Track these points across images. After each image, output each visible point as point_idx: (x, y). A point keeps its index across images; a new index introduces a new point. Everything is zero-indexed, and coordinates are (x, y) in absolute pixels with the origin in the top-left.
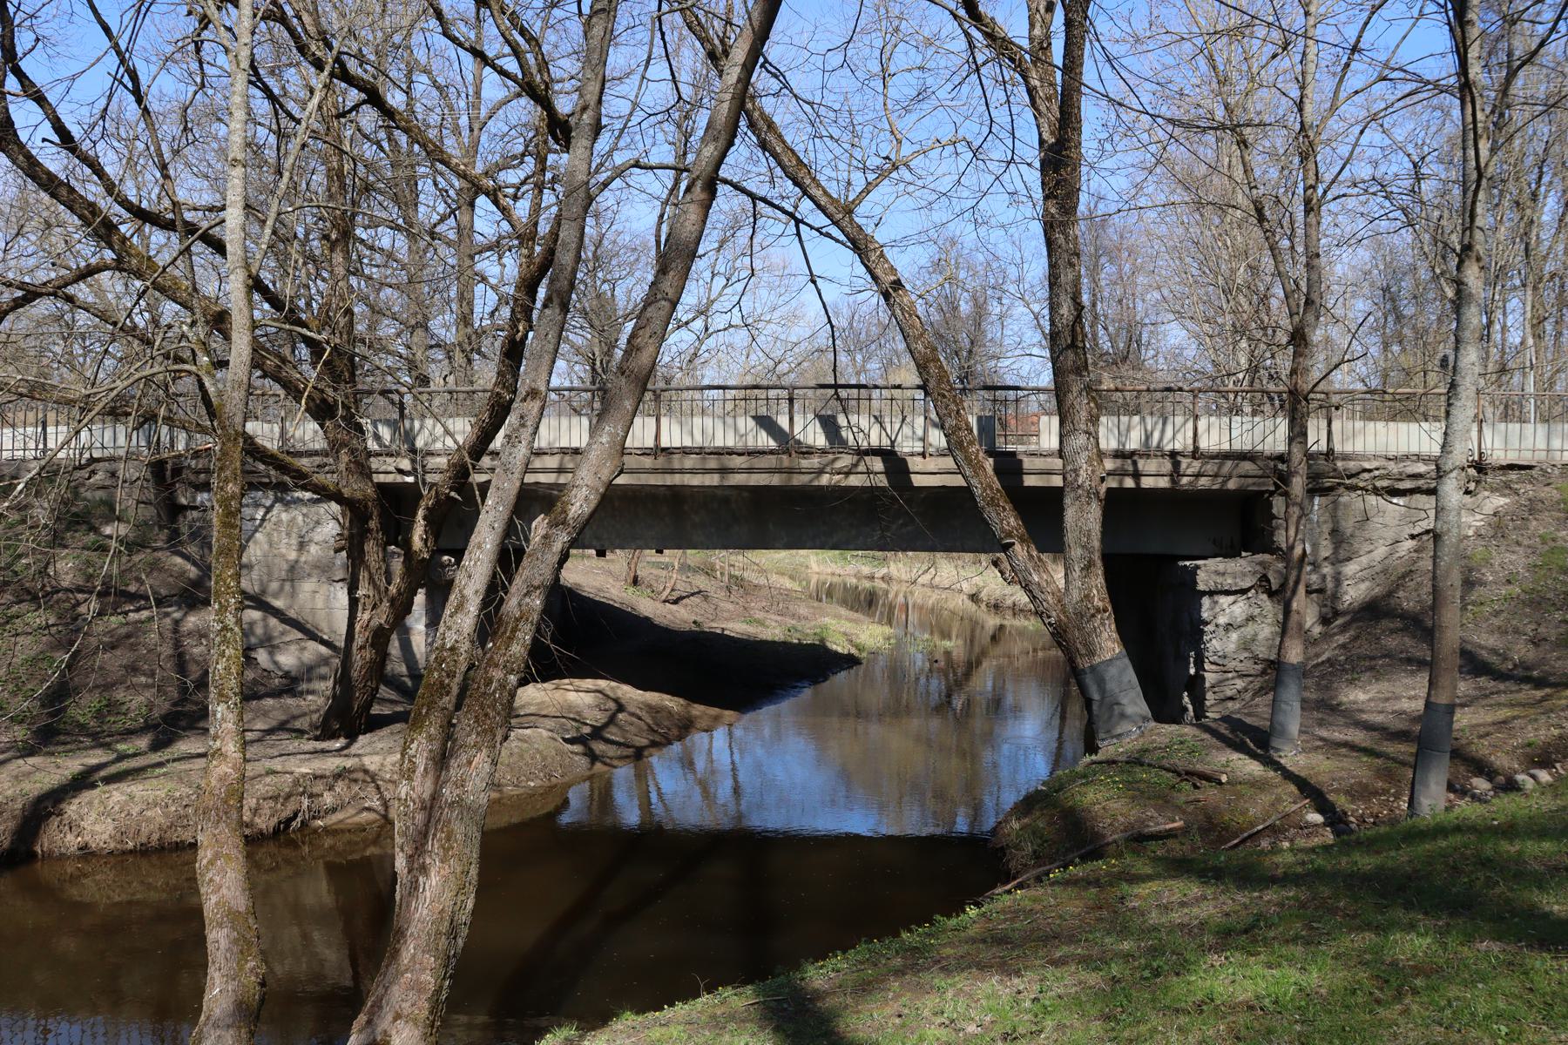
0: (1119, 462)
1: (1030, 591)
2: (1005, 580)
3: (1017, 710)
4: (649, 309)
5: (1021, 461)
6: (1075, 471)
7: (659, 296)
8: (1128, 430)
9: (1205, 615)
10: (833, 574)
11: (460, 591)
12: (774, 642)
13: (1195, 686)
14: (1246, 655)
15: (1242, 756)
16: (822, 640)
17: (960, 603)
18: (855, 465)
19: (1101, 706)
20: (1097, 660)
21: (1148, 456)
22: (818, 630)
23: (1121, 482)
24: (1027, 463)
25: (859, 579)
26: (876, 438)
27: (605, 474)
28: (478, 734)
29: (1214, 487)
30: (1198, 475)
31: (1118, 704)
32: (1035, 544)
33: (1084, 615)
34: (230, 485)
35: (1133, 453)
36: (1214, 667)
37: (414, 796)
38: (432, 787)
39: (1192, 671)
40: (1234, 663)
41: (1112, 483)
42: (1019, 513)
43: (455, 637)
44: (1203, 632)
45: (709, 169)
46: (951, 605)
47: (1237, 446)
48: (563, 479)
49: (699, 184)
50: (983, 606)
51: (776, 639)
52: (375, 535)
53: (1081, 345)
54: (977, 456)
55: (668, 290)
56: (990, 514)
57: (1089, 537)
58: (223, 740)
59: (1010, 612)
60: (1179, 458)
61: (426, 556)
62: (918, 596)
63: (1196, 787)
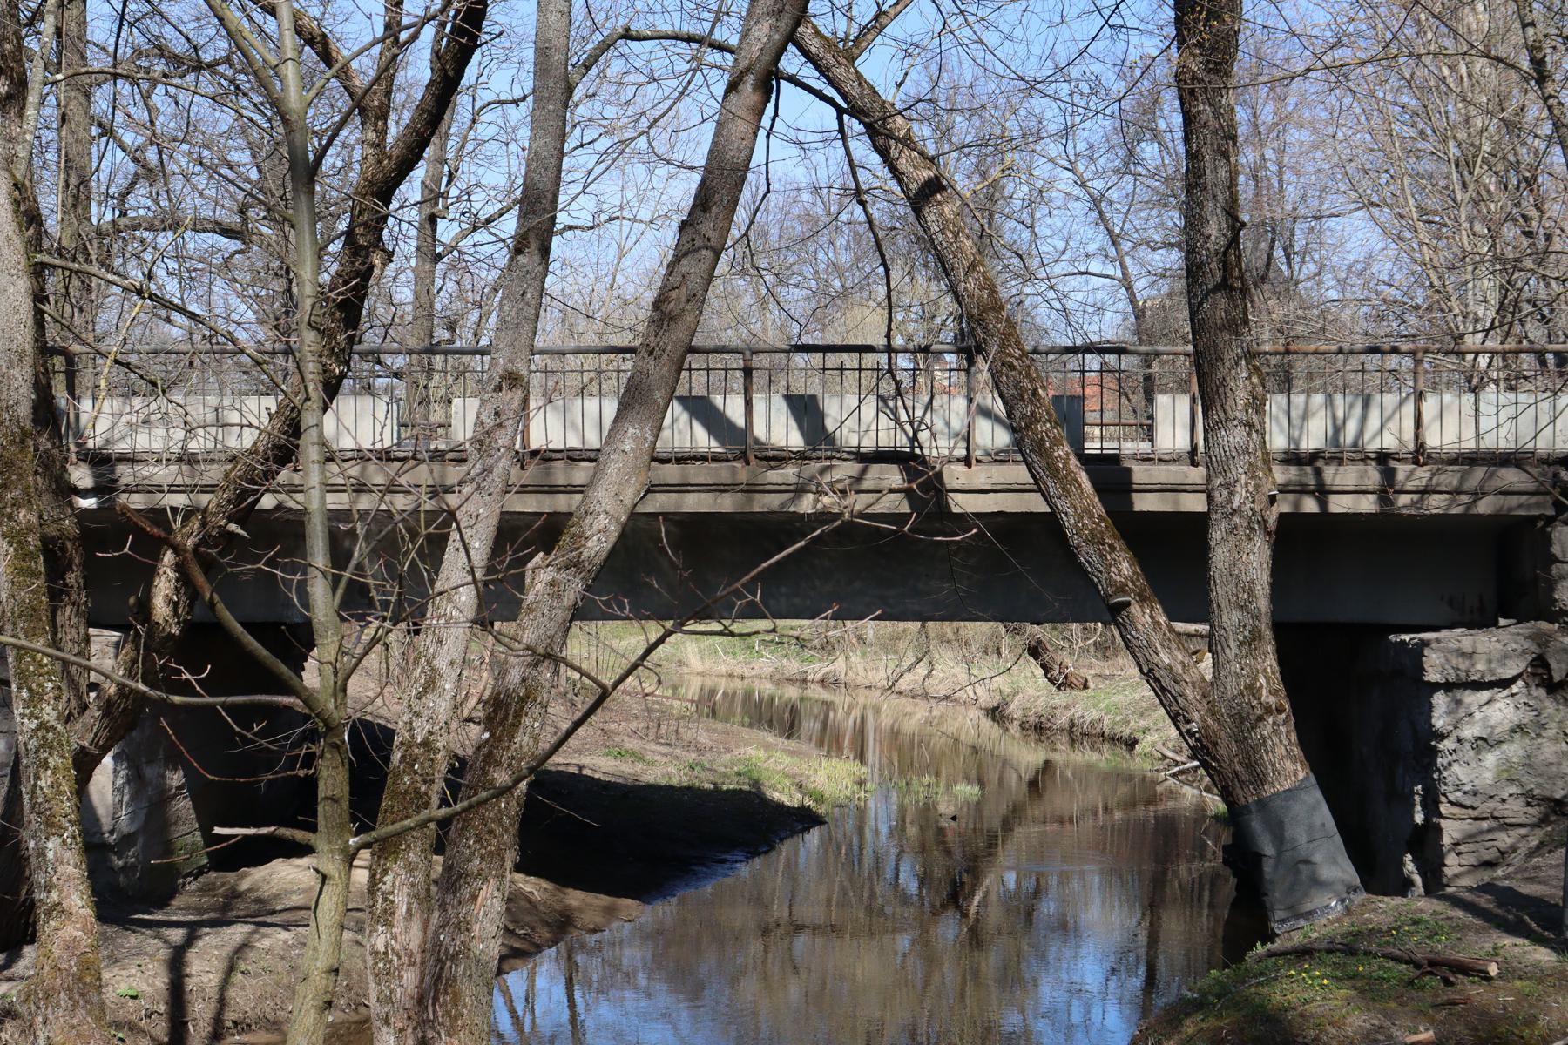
0: (1293, 471)
1: (1157, 680)
2: (1051, 681)
3: (1065, 928)
4: (684, 261)
5: (1129, 471)
6: (1227, 486)
7: (698, 243)
8: (1305, 416)
9: (1440, 721)
10: (730, 675)
11: (429, 663)
12: (671, 788)
13: (1426, 843)
14: (1513, 790)
15: (1519, 941)
16: (756, 783)
17: (970, 724)
18: (859, 479)
19: (1276, 867)
20: (1269, 790)
21: (1340, 462)
22: (742, 768)
23: (1297, 504)
24: (1140, 474)
25: (778, 683)
26: (885, 435)
27: (629, 496)
28: (482, 858)
29: (1455, 511)
30: (1425, 492)
31: (1307, 862)
32: (1161, 603)
33: (1244, 721)
34: (23, 512)
35: (1315, 456)
36: (1456, 810)
37: (397, 947)
38: (420, 934)
39: (1419, 818)
40: (1491, 804)
41: (1284, 507)
42: (1136, 555)
43: (428, 727)
44: (1435, 752)
45: (766, 59)
46: (951, 727)
47: (1488, 443)
48: (561, 503)
49: (750, 79)
50: (1014, 729)
51: (675, 782)
52: (74, 597)
53: (1238, 284)
54: (1066, 464)
55: (710, 233)
56: (1088, 555)
57: (1251, 592)
58: (61, 891)
59: (1065, 738)
60: (1393, 464)
61: (175, 630)
62: (890, 711)
63: (1447, 982)
